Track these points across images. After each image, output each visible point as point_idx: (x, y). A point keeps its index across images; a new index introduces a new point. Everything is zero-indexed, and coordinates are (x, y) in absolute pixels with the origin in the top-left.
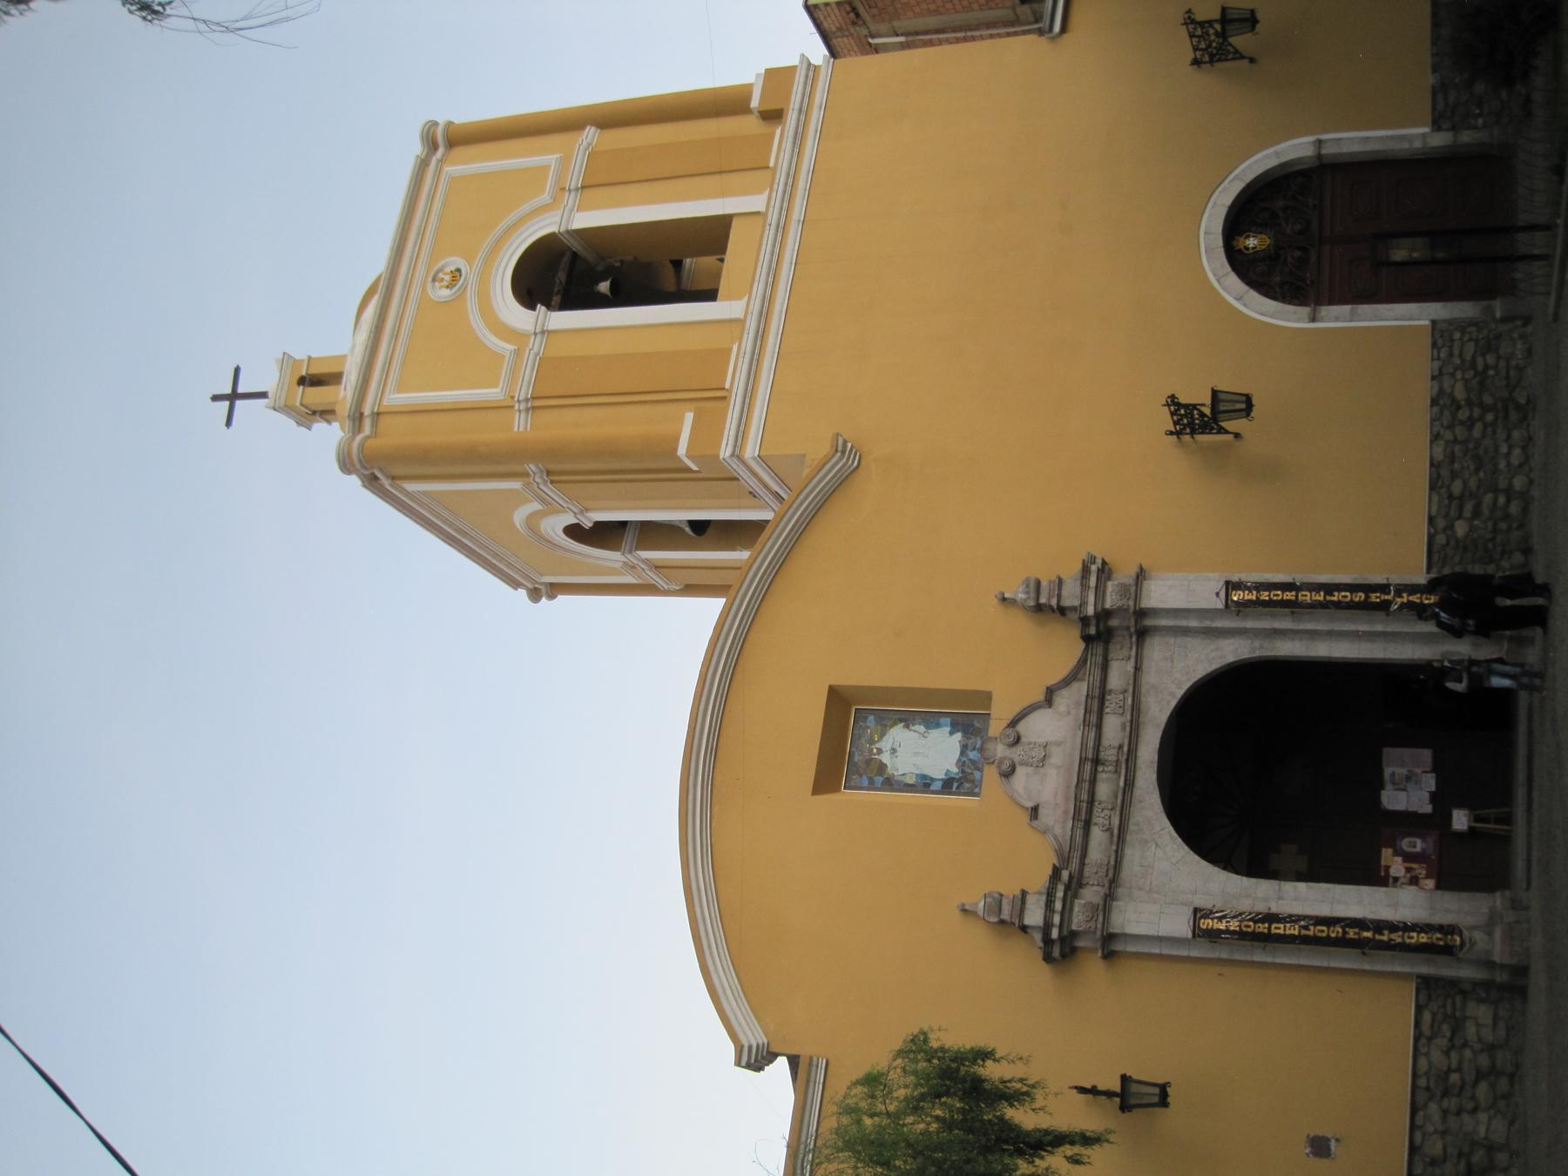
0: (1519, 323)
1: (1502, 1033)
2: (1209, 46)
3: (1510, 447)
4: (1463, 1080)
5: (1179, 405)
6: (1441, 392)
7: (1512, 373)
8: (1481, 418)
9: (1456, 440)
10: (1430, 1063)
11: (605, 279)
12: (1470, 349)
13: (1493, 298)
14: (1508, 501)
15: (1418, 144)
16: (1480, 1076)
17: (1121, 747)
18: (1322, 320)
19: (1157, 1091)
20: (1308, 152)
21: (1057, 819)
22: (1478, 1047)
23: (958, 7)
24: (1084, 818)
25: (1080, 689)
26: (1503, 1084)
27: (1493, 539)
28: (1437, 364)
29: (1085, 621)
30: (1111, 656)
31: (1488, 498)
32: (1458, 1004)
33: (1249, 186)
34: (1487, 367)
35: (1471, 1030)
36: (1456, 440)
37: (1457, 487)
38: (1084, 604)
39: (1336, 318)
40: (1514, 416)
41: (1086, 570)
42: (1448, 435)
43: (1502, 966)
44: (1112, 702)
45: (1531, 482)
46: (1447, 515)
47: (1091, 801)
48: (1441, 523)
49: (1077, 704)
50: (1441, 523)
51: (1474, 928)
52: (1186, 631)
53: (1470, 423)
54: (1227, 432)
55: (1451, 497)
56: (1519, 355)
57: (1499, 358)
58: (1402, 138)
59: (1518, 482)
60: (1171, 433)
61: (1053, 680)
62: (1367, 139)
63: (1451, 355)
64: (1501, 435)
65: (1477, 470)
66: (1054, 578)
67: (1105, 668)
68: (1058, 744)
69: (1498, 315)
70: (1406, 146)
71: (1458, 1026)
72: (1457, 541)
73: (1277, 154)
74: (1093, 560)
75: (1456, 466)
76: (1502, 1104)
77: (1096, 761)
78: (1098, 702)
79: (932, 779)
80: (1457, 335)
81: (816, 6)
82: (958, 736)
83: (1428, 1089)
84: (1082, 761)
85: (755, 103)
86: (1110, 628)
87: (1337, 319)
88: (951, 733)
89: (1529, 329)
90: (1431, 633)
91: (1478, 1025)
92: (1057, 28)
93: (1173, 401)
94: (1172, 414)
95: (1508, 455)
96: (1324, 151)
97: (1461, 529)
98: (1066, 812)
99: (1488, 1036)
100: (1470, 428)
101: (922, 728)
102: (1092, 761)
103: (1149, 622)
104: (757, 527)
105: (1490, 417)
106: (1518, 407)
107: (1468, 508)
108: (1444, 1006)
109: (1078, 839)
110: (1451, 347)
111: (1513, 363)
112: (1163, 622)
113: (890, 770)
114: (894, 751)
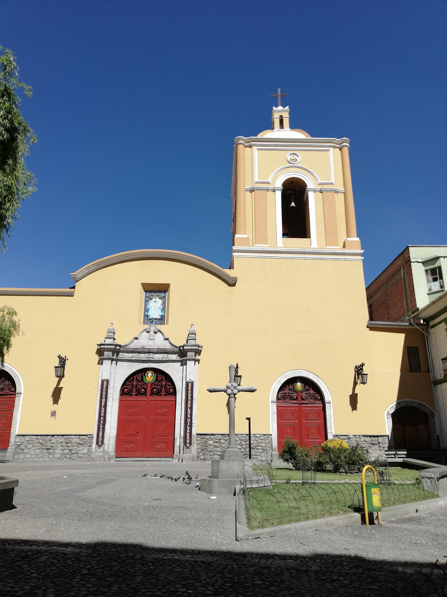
5: (362, 366)
21: (136, 345)
22: (77, 450)
25: (167, 346)
26: (68, 456)
34: (258, 449)
35: (81, 448)
37: (222, 441)
39: (273, 408)
44: (166, 355)
51: (104, 448)
61: (170, 340)
80: (267, 441)
82: (159, 317)
86: (183, 354)
93: (363, 365)
94: (360, 365)
97: (211, 442)
98: (136, 346)
100: (239, 445)
101: (161, 308)
113: (150, 301)
114: (155, 301)
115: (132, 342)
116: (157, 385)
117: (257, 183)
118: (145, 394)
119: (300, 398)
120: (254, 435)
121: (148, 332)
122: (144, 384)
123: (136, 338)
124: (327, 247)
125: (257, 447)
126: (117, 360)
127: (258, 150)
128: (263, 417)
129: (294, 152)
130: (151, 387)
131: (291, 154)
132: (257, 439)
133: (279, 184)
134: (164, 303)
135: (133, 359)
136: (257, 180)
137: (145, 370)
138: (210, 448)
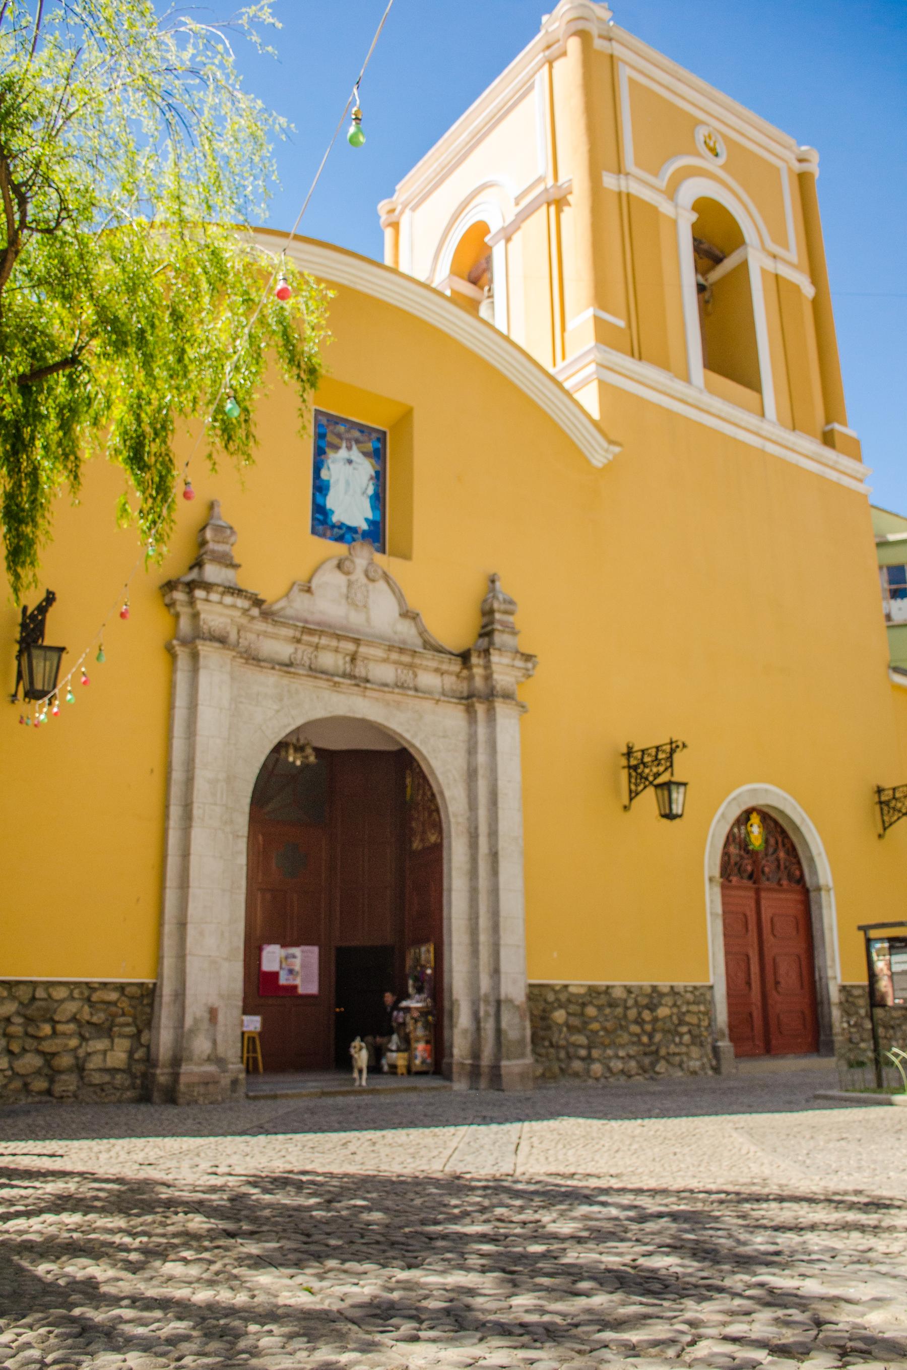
0: (714, 1063)
1: (97, 1078)
2: (645, 765)
4: (45, 1038)
5: (672, 752)
6: (661, 995)
7: (677, 1058)
8: (643, 1031)
9: (626, 1008)
10: (62, 1001)
13: (732, 1039)
15: (830, 973)
16: (49, 1057)
18: (711, 888)
19: (680, 812)
20: (822, 882)
22: (81, 1053)
26: (40, 1084)
28: (682, 990)
31: (581, 1039)
32: (127, 1030)
35: (99, 1045)
36: (626, 1008)
37: (591, 1011)
40: (647, 1061)
42: (630, 1002)
43: (176, 1076)
45: (597, 1079)
46: (569, 1001)
50: (563, 997)
52: (472, 751)
53: (639, 1021)
54: (631, 799)
55: (584, 1005)
57: (687, 1046)
58: (833, 960)
59: (597, 1068)
62: (831, 929)
63: (688, 1003)
64: (632, 1050)
68: (368, 620)
69: (720, 1044)
70: (829, 963)
71: (106, 1030)
72: (551, 1011)
73: (819, 854)
76: (17, 1084)
79: (326, 495)
82: (365, 526)
83: (33, 999)
87: (712, 901)
88: (367, 520)
90: (479, 988)
91: (105, 1052)
95: (617, 1057)
99: (94, 1063)
100: (636, 1022)
105: (645, 1039)
106: (653, 1064)
107: (575, 1022)
108: (124, 1014)
109: (351, 635)
110: (694, 1003)
111: (685, 1059)
112: (482, 731)
114: (350, 462)
134: (379, 478)
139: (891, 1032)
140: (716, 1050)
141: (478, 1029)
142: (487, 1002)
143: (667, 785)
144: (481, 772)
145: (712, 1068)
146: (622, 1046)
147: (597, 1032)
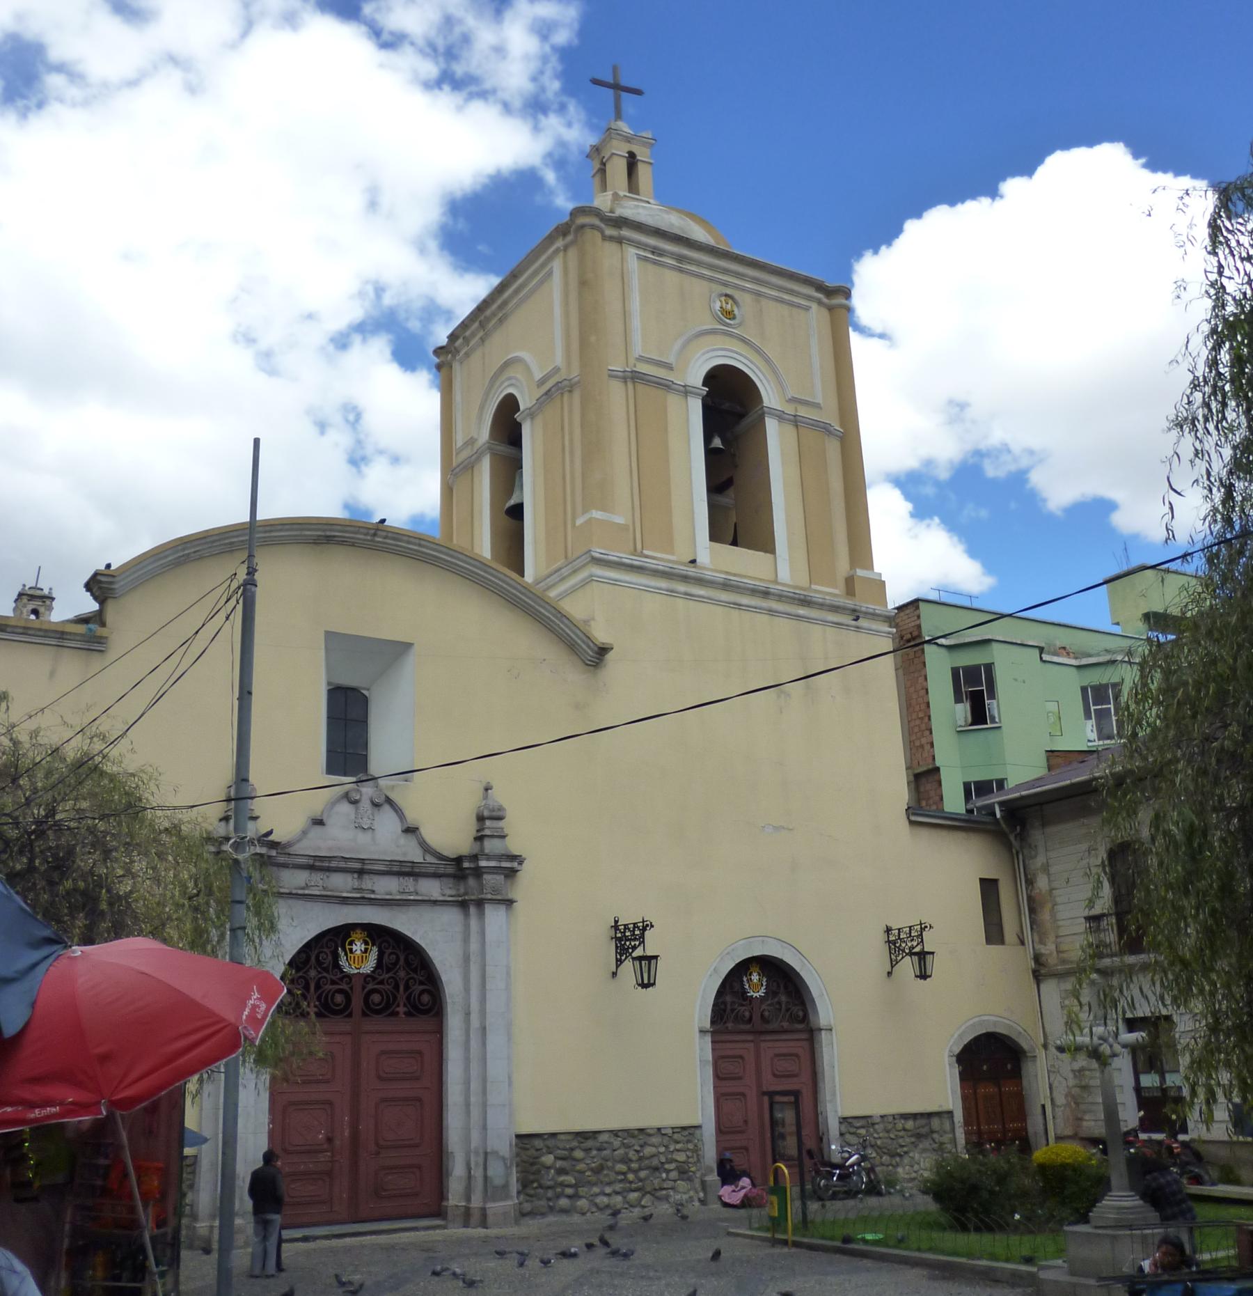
0: (701, 1195)
3: (608, 1195)
5: (644, 929)
8: (630, 1169)
11: (723, 443)
12: (681, 1157)
14: (569, 1197)
17: (373, 892)
21: (318, 844)
23: (912, 724)
24: (318, 865)
25: (416, 855)
27: (540, 1186)
28: (670, 1131)
29: (474, 858)
30: (445, 880)
31: (570, 1179)
33: (781, 961)
34: (668, 1171)
37: (578, 1154)
38: (489, 857)
41: (513, 858)
44: (409, 883)
47: (329, 870)
48: (551, 1143)
49: (405, 854)
56: (678, 1197)
57: (675, 1181)
59: (582, 1203)
60: (616, 922)
65: (592, 1170)
66: (506, 831)
67: (436, 876)
74: (521, 863)
75: (594, 1152)
77: (361, 873)
78: (407, 871)
80: (690, 1146)
81: (918, 608)
84: (362, 861)
85: (860, 572)
87: (701, 1050)
89: (697, 1204)
92: (913, 818)
93: (646, 927)
96: (823, 1033)
97: (548, 1159)
102: (362, 869)
103: (473, 910)
104: (518, 565)
115: (305, 833)
116: (381, 982)
117: (641, 359)
118: (345, 1011)
119: (756, 1018)
120: (659, 1129)
121: (355, 802)
122: (341, 979)
123: (319, 822)
124: (814, 587)
125: (667, 1166)
126: (480, 904)
127: (639, 257)
128: (666, 1079)
129: (729, 291)
130: (364, 988)
131: (721, 295)
132: (666, 1140)
133: (696, 377)
135: (306, 892)
136: (638, 349)
137: (338, 936)
138: (549, 1177)
139: (898, 1159)
140: (703, 1183)
141: (469, 1177)
142: (477, 1153)
143: (640, 959)
144: (473, 958)
145: (700, 1200)
146: (609, 1184)
147: (584, 1172)
